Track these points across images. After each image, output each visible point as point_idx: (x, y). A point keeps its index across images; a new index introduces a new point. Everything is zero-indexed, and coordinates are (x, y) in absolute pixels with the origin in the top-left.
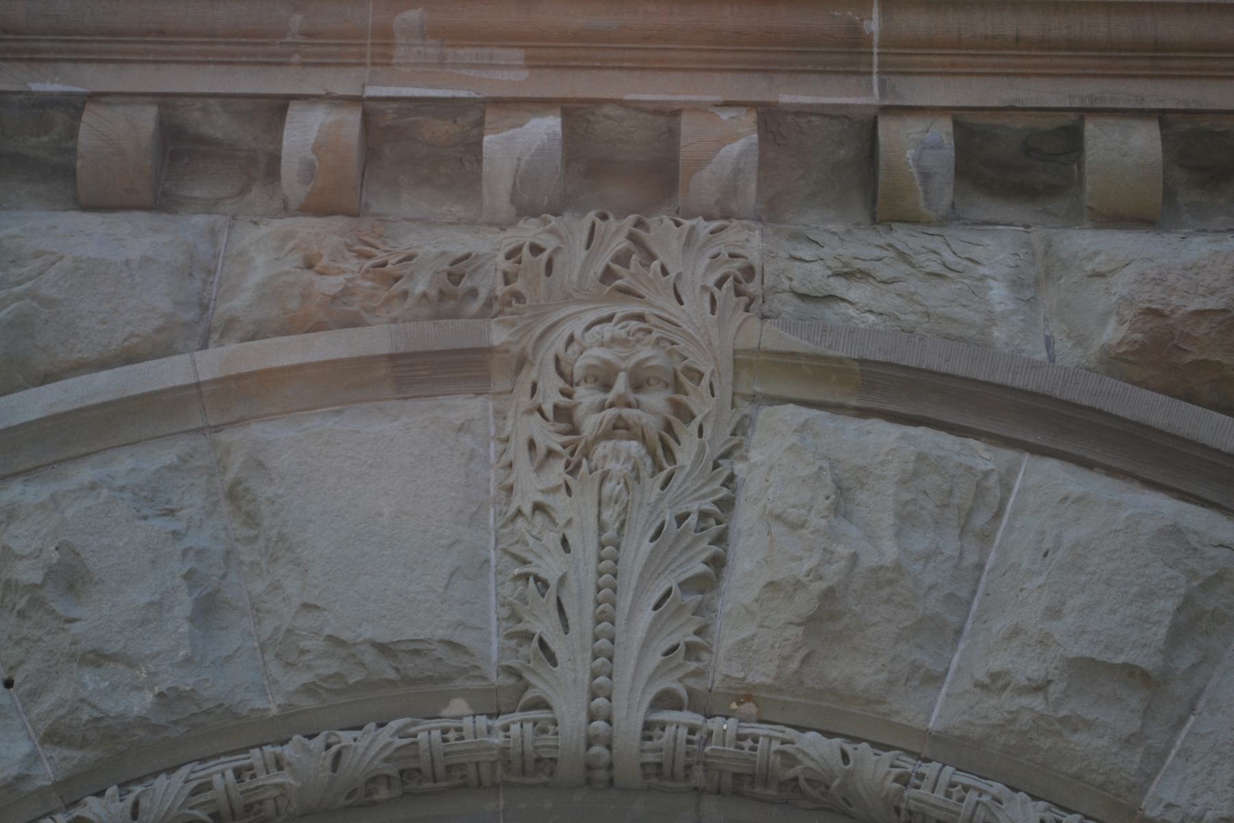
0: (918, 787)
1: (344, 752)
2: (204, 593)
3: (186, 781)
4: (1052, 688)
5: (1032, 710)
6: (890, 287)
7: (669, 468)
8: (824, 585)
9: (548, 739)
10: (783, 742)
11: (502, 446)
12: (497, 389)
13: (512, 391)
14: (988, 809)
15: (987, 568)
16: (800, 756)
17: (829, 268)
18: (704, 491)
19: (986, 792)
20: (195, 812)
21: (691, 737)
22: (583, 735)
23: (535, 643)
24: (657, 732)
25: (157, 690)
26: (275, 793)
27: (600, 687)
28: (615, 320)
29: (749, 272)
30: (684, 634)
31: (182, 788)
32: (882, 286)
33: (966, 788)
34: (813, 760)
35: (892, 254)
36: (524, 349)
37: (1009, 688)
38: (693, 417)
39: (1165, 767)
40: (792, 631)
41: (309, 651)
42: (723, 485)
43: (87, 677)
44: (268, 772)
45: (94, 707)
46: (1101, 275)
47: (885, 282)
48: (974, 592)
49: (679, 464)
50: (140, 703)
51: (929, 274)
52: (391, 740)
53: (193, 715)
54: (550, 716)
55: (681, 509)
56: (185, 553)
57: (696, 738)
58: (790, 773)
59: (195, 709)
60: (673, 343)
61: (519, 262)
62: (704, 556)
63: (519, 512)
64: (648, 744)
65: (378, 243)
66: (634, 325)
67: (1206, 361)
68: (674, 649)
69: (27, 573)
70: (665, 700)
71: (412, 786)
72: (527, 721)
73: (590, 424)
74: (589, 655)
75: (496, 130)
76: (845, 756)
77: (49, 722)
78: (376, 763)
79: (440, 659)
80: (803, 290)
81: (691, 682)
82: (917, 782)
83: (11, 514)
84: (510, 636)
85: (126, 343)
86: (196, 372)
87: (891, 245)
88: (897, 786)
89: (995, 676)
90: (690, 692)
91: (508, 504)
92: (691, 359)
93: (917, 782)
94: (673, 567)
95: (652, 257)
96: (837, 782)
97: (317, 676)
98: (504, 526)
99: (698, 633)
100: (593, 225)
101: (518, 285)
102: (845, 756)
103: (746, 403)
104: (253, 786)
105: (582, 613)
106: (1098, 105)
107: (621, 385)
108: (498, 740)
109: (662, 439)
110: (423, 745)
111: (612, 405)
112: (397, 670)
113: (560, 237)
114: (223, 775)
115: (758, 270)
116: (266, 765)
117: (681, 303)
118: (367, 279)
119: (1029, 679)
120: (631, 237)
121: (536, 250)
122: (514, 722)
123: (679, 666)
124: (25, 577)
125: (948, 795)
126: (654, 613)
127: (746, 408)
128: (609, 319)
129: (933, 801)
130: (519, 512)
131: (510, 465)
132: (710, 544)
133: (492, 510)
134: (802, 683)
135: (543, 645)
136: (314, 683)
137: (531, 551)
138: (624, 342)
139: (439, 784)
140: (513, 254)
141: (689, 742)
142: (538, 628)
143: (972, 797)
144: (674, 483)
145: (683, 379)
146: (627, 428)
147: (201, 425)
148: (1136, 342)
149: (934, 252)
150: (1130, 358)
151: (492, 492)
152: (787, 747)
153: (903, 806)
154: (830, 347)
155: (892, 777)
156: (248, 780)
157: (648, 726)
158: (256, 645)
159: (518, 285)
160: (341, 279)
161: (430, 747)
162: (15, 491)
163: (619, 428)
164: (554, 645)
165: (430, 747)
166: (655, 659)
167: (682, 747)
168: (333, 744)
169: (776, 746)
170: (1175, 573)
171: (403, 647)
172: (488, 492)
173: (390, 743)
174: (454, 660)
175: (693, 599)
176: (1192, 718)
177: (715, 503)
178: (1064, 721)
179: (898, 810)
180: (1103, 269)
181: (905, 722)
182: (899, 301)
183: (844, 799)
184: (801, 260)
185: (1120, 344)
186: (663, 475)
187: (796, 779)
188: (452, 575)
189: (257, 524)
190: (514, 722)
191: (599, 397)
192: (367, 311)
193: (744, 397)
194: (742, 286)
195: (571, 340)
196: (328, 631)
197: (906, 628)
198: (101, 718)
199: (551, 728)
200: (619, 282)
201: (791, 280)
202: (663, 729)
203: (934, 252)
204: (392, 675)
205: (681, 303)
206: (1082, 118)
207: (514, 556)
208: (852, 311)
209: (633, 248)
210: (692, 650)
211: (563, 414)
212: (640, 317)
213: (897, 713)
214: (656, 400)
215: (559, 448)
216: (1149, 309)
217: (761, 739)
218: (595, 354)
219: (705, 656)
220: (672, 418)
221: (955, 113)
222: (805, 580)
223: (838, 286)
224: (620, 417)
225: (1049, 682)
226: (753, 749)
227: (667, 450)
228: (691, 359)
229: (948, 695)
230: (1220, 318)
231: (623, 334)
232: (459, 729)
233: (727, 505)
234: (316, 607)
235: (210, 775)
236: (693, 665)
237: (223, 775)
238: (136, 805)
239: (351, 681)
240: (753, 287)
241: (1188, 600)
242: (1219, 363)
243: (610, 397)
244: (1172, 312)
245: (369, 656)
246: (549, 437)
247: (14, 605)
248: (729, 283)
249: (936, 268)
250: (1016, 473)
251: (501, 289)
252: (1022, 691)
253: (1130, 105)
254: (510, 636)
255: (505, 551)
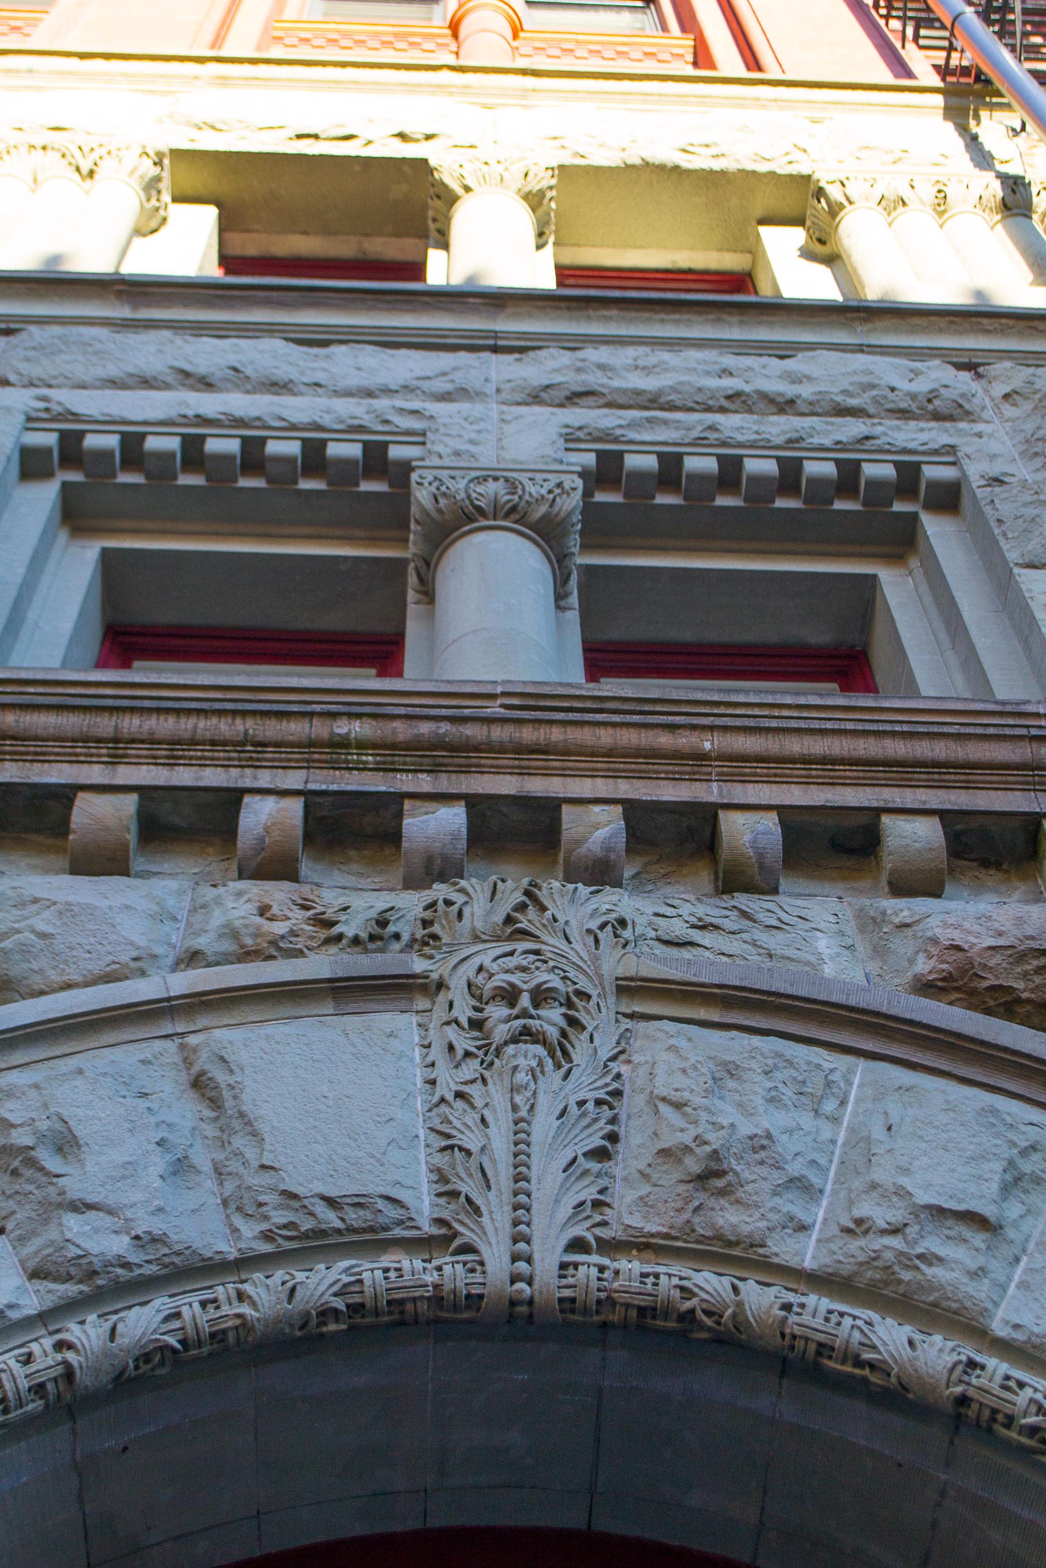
0: (800, 1314)
1: (298, 1287)
2: (174, 1158)
3: (159, 1311)
4: (908, 1230)
5: (893, 1249)
6: (738, 936)
7: (567, 1066)
8: (708, 1149)
9: (478, 1278)
10: (681, 1278)
11: (425, 1050)
12: (419, 1008)
13: (431, 1011)
14: (862, 1331)
15: (839, 1143)
16: (696, 1290)
17: (687, 922)
18: (597, 1084)
19: (859, 1318)
20: (166, 1337)
21: (600, 1275)
22: (508, 1274)
23: (462, 1199)
24: (571, 1271)
25: (133, 1233)
26: (238, 1322)
27: (520, 1233)
28: (516, 954)
29: (622, 922)
30: (590, 1193)
31: (154, 1316)
32: (731, 936)
33: (842, 1314)
34: (707, 1292)
35: (736, 913)
36: (441, 976)
37: (871, 1232)
38: (584, 1028)
39: (1007, 1297)
40: (682, 1188)
41: (266, 1204)
42: (613, 1080)
43: (72, 1221)
44: (230, 1304)
45: (78, 1246)
46: (907, 925)
47: (733, 933)
48: (831, 1161)
49: (575, 1063)
50: (119, 1245)
51: (768, 926)
52: (339, 1277)
53: (165, 1255)
54: (477, 1258)
55: (580, 1096)
56: (157, 1125)
57: (605, 1275)
58: (688, 1305)
59: (167, 1251)
60: (565, 971)
61: (435, 911)
62: (601, 1133)
63: (443, 1100)
64: (564, 1282)
65: (317, 900)
66: (532, 957)
67: (1000, 986)
68: (582, 1204)
69: (21, 1138)
70: (578, 1245)
71: (358, 1320)
72: (458, 1262)
73: (501, 1032)
74: (510, 1207)
75: (413, 816)
76: (735, 1289)
77: (37, 1260)
78: (326, 1297)
79: (380, 1211)
80: (666, 938)
81: (597, 1231)
82: (799, 1310)
83: (9, 1093)
84: (439, 1195)
85: (108, 969)
86: (167, 989)
87: (734, 907)
88: (783, 1313)
89: (859, 1222)
90: (598, 1239)
91: (433, 1094)
92: (581, 984)
93: (799, 1310)
94: (576, 1141)
95: (543, 909)
96: (729, 1311)
97: (274, 1224)
98: (430, 1110)
99: (601, 1192)
100: (495, 884)
101: (436, 929)
102: (735, 1289)
103: (627, 1020)
104: (217, 1316)
105: (502, 1174)
106: (890, 805)
107: (525, 1001)
108: (431, 1278)
109: (560, 1044)
110: (367, 1282)
111: (517, 1017)
112: (342, 1219)
113: (467, 894)
114: (191, 1306)
115: (630, 922)
116: (229, 1299)
117: (570, 943)
118: (309, 924)
119: (888, 1223)
120: (527, 893)
121: (448, 903)
122: (446, 1264)
123: (588, 1217)
124: (18, 1141)
125: (827, 1320)
126: (563, 1175)
127: (627, 1023)
128: (511, 954)
129: (814, 1326)
130: (443, 1100)
131: (433, 1065)
132: (606, 1124)
133: (419, 1099)
134: (693, 1231)
135: (469, 1200)
136: (270, 1231)
137: (455, 1128)
138: (524, 969)
139: (380, 1319)
140: (431, 906)
141: (599, 1279)
142: (463, 1188)
143: (847, 1322)
144: (572, 1077)
145: (575, 999)
146: (530, 1034)
147: (170, 1032)
148: (943, 971)
149: (770, 911)
150: (940, 984)
151: (419, 1086)
152: (684, 1283)
153: (788, 1331)
154: (695, 975)
155: (777, 1306)
156: (212, 1311)
157: (563, 1266)
158: (219, 1201)
159: (436, 929)
160: (288, 923)
161: (374, 1283)
162: (13, 1077)
163: (526, 1035)
164: (479, 1201)
165: (374, 1283)
166: (565, 1210)
167: (594, 1284)
168: (287, 1281)
169: (675, 1281)
170: (998, 1142)
171: (349, 1200)
172: (415, 1085)
173: (339, 1280)
174: (392, 1212)
175: (594, 1166)
176: (1025, 1258)
177: (608, 1093)
178: (920, 1257)
179: (783, 1335)
180: (908, 921)
181: (784, 1263)
182: (745, 946)
183: (735, 1327)
184: (663, 916)
185: (930, 972)
186: (563, 1070)
187: (692, 1311)
188: (389, 1144)
189: (219, 1107)
190: (446, 1264)
191: (505, 1012)
192: (309, 949)
193: (625, 1015)
194: (618, 932)
195: (481, 969)
196: (282, 1187)
197: (779, 1185)
198: (84, 1256)
199: (478, 1267)
200: (519, 925)
201: (656, 930)
202: (576, 1269)
203: (770, 911)
204: (339, 1224)
205: (570, 943)
206: (878, 817)
207: (439, 1133)
208: (707, 953)
209: (528, 902)
210: (597, 1204)
211: (476, 1024)
212: (537, 952)
213: (776, 1255)
214: (553, 1016)
215: (474, 1050)
216: (951, 945)
217: (662, 1276)
218: (500, 980)
219: (607, 1210)
220: (568, 1028)
221: (783, 811)
222: (693, 1145)
223: (697, 936)
224: (524, 1026)
225: (906, 1225)
226: (655, 1284)
227: (565, 1053)
228: (581, 984)
229: (819, 1241)
230: (1009, 952)
231: (524, 963)
232: (397, 1270)
233: (617, 1094)
234: (272, 1168)
235: (178, 1307)
236: (598, 1218)
237: (191, 1306)
238: (113, 1330)
239: (303, 1229)
240: (627, 934)
241: (1011, 1163)
242: (1010, 987)
243: (515, 1011)
244: (971, 947)
245: (321, 1209)
246: (463, 1042)
247: (8, 1166)
248: (609, 928)
249: (775, 923)
250: (855, 1073)
251: (420, 933)
252: (884, 1232)
253: (916, 806)
254: (439, 1195)
255: (432, 1129)
